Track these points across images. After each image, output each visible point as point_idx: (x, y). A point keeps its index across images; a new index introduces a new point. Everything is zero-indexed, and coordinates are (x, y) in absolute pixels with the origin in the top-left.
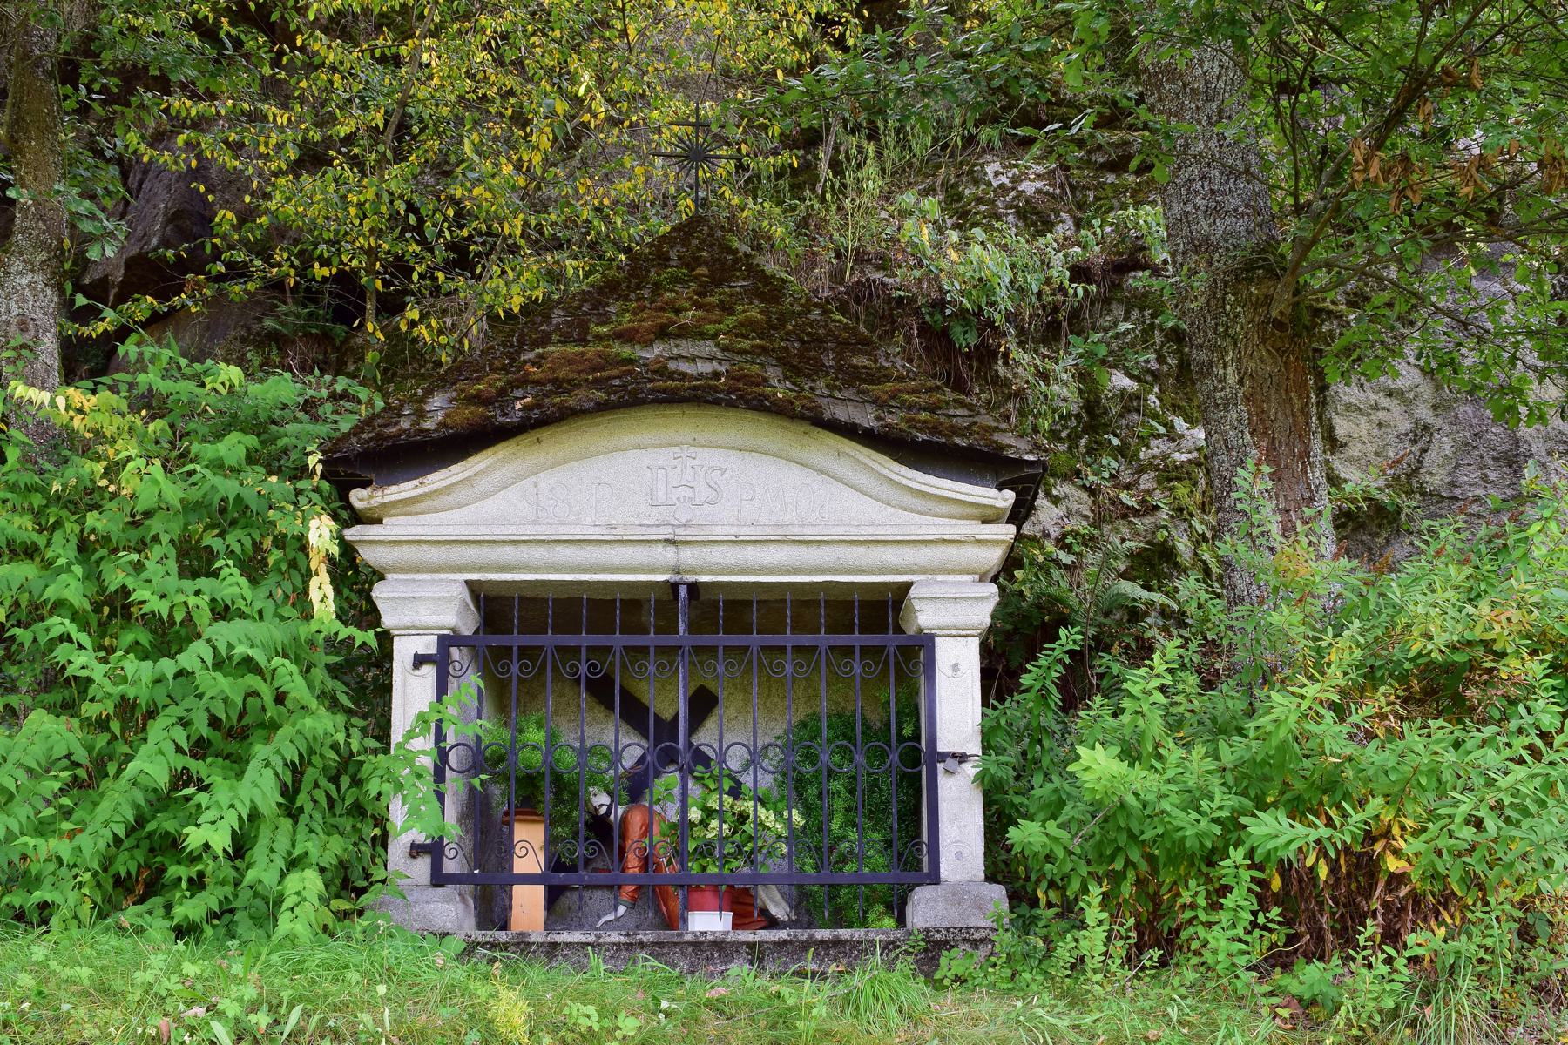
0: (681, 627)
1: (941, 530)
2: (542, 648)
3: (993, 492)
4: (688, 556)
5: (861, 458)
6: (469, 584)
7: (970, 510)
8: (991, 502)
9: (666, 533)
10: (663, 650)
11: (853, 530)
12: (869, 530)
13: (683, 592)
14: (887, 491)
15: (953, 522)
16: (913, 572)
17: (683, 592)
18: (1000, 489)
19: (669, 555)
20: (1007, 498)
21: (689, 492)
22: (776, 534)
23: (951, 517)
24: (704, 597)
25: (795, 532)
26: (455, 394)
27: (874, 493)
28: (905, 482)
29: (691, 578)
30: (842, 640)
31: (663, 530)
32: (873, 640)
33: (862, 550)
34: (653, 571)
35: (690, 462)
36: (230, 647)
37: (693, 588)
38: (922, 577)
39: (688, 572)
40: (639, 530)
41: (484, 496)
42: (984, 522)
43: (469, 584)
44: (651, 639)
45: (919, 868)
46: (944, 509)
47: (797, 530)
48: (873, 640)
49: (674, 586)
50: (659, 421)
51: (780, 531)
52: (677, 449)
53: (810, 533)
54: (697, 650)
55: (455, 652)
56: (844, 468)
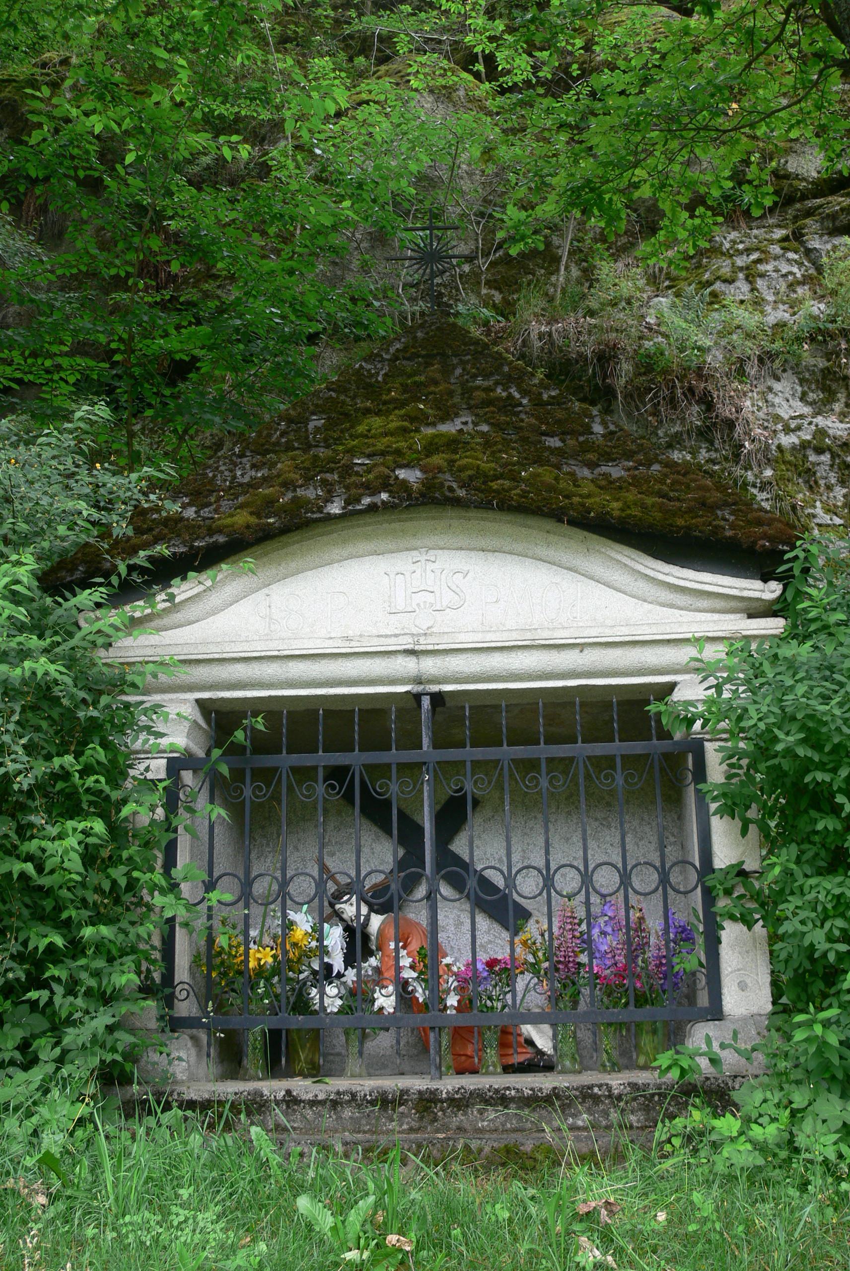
0: (426, 741)
1: (704, 627)
2: (276, 769)
3: (758, 584)
4: (430, 666)
5: (619, 557)
6: (201, 704)
7: (733, 604)
8: (757, 595)
9: (407, 643)
10: (404, 767)
11: (608, 632)
12: (625, 630)
13: (426, 702)
14: (642, 586)
15: (716, 616)
16: (676, 672)
17: (426, 702)
18: (765, 581)
19: (409, 666)
20: (771, 591)
21: (430, 598)
22: (525, 638)
23: (713, 611)
24: (449, 703)
25: (544, 635)
26: (219, 1208)
27: (628, 589)
28: (661, 577)
29: (435, 688)
30: (599, 749)
31: (401, 640)
32: (637, 747)
33: (618, 652)
34: (393, 682)
35: (431, 566)
36: (15, 598)
37: (438, 699)
38: (687, 677)
39: (431, 681)
40: (376, 641)
41: (215, 612)
42: (750, 616)
43: (201, 704)
44: (394, 756)
45: (691, 998)
46: (705, 603)
47: (546, 634)
48: (637, 747)
49: (418, 697)
50: (394, 525)
51: (529, 635)
52: (415, 553)
53: (561, 636)
54: (443, 765)
55: (187, 777)
56: (595, 565)
